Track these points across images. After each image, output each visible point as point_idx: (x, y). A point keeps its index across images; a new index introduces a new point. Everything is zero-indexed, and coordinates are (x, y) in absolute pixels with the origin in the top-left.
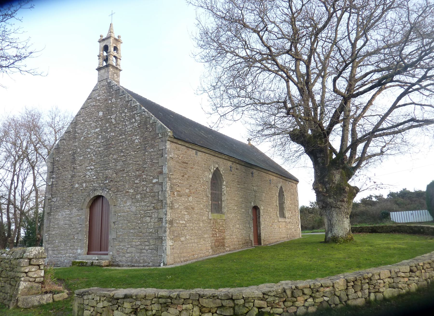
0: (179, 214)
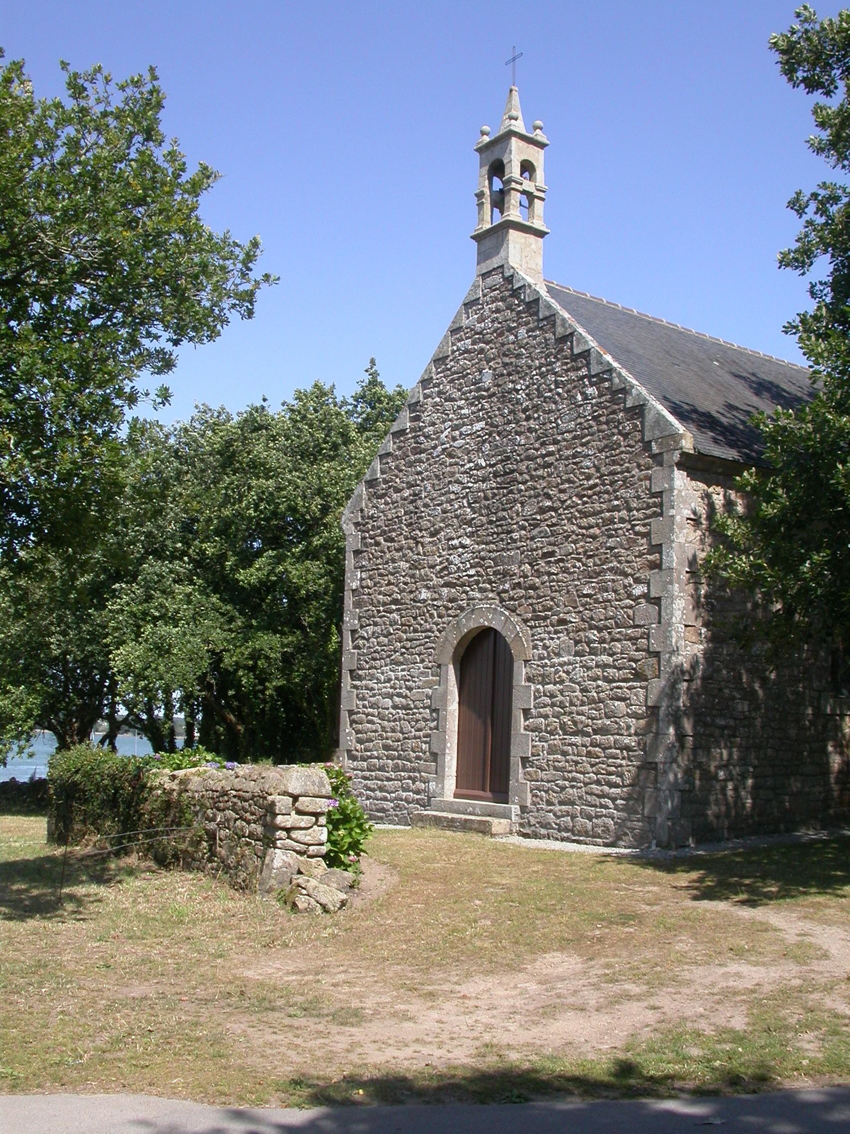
0: (714, 697)
